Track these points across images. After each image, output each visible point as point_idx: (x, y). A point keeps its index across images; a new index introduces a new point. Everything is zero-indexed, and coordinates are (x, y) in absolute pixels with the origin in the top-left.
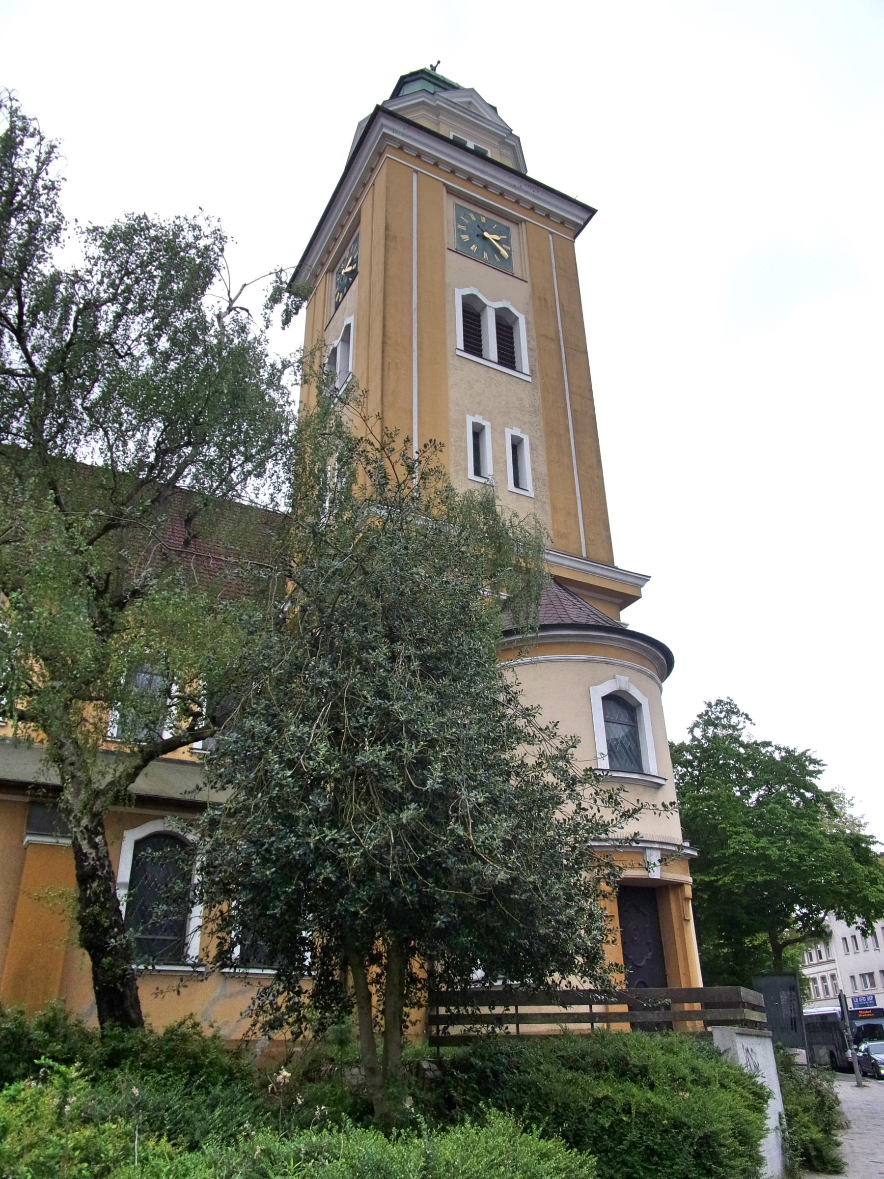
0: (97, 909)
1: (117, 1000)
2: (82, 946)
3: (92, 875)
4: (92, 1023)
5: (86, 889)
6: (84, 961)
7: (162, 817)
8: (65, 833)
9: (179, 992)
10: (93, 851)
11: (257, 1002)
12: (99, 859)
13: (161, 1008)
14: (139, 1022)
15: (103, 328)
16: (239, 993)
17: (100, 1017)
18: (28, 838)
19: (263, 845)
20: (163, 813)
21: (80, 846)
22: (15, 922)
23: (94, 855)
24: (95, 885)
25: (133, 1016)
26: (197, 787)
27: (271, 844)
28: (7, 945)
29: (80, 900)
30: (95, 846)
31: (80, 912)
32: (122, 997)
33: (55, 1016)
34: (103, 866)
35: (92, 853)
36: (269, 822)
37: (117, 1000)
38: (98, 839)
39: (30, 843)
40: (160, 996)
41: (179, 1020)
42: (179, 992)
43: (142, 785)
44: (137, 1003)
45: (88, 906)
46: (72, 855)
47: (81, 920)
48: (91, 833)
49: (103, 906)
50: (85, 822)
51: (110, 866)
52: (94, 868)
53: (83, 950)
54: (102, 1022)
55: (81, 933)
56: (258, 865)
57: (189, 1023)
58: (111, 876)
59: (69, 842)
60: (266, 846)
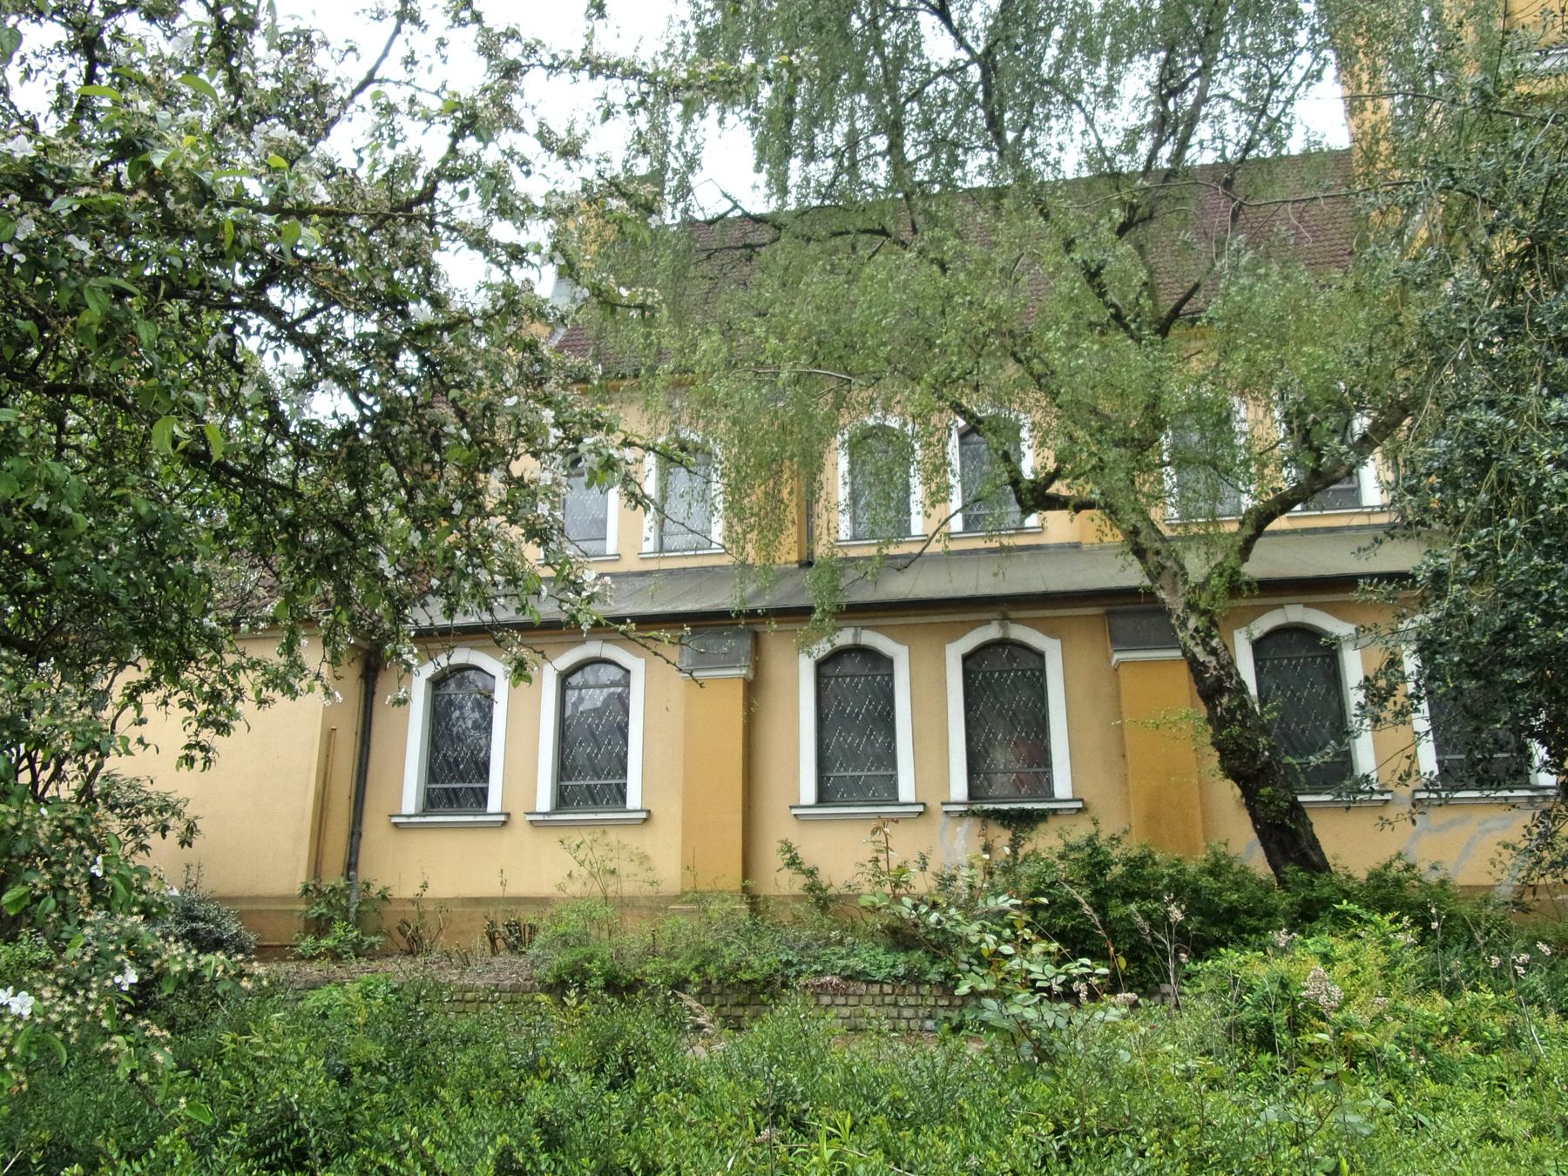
0: (1236, 730)
1: (1287, 839)
2: (1227, 777)
3: (1213, 687)
4: (1259, 865)
5: (1215, 707)
6: (1229, 792)
7: (1281, 606)
8: (1173, 643)
9: (1414, 822)
10: (1212, 658)
11: (1536, 830)
12: (1223, 667)
13: (1350, 844)
14: (1322, 866)
15: (1045, 70)
16: (1452, 823)
17: (1270, 861)
18: (1117, 656)
19: (1539, 594)
20: (1276, 601)
21: (1194, 655)
22: (1129, 757)
23: (1214, 663)
24: (1225, 700)
25: (1315, 859)
26: (1376, 540)
27: (1552, 594)
28: (1125, 783)
29: (1209, 720)
30: (1213, 652)
31: (1213, 736)
32: (1294, 835)
33: (1218, 861)
34: (1230, 676)
35: (1212, 661)
36: (1536, 560)
37: (1287, 839)
38: (1214, 643)
39: (1120, 663)
40: (1388, 828)
41: (1383, 862)
42: (1414, 822)
43: (1255, 568)
44: (1315, 843)
45: (1224, 727)
46: (1184, 669)
47: (1217, 745)
48: (1205, 636)
49: (1242, 724)
50: (1193, 623)
51: (1238, 674)
52: (1219, 679)
53: (1229, 782)
54: (1275, 868)
55: (1222, 761)
56: (1538, 625)
57: (1398, 864)
58: (1242, 687)
59: (1177, 654)
60: (1545, 596)
